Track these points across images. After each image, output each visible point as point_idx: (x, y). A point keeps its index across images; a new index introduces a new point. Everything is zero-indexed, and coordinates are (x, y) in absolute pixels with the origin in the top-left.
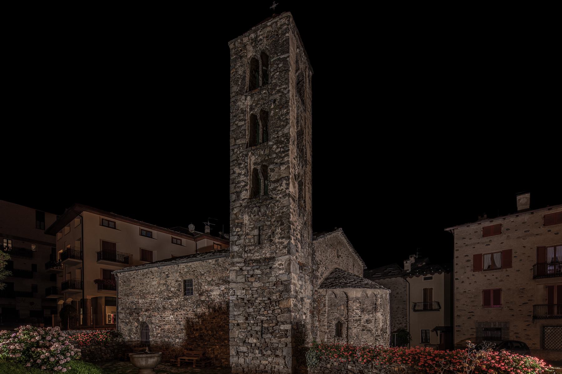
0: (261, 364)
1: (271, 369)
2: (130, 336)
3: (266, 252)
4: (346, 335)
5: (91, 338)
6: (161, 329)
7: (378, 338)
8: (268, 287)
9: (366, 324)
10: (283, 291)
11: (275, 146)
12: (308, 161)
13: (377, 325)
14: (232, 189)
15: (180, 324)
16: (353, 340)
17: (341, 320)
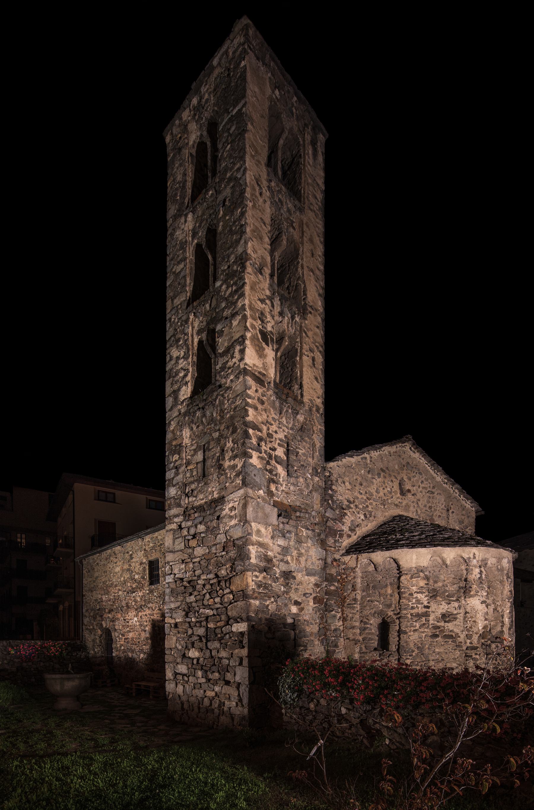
0: (206, 697)
1: (219, 706)
2: (94, 650)
3: (214, 489)
4: (397, 647)
5: (37, 651)
7: (473, 653)
8: (215, 554)
9: (442, 624)
10: (235, 560)
11: (224, 287)
12: (311, 307)
13: (469, 625)
14: (168, 390)
15: (145, 631)
16: (410, 656)
17: (387, 615)
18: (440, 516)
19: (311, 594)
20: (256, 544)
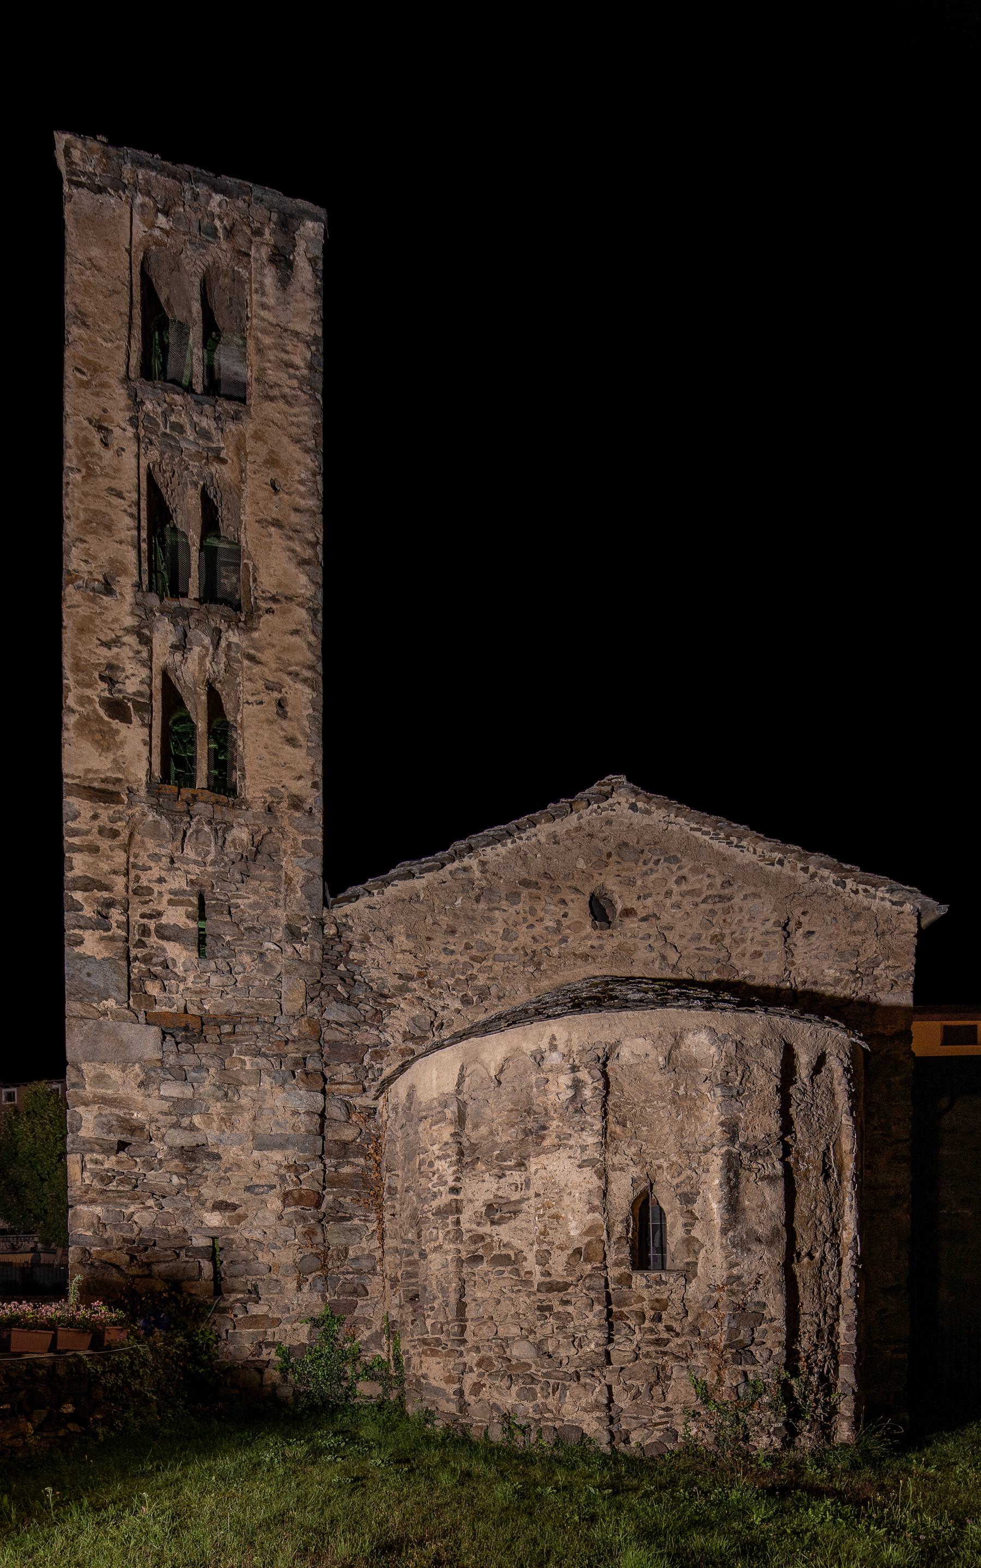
9: (487, 1229)
20: (95, 1102)
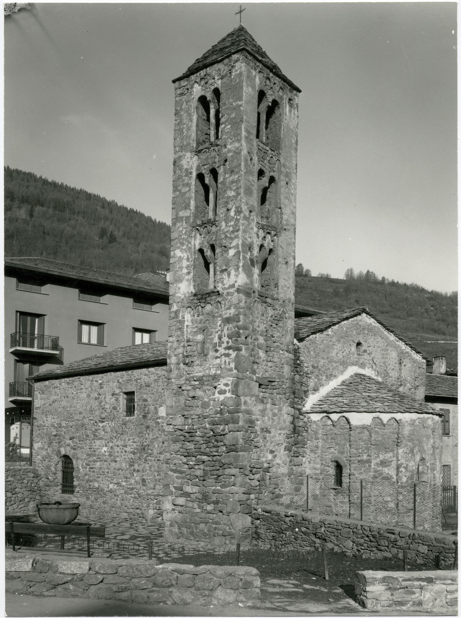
3: (211, 366)
6: (90, 468)
18: (393, 369)
19: (283, 444)
